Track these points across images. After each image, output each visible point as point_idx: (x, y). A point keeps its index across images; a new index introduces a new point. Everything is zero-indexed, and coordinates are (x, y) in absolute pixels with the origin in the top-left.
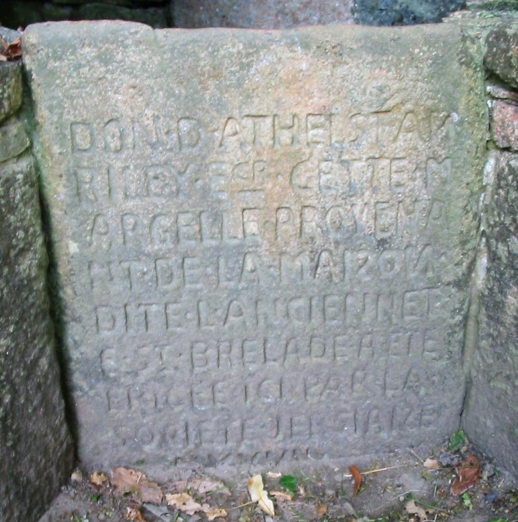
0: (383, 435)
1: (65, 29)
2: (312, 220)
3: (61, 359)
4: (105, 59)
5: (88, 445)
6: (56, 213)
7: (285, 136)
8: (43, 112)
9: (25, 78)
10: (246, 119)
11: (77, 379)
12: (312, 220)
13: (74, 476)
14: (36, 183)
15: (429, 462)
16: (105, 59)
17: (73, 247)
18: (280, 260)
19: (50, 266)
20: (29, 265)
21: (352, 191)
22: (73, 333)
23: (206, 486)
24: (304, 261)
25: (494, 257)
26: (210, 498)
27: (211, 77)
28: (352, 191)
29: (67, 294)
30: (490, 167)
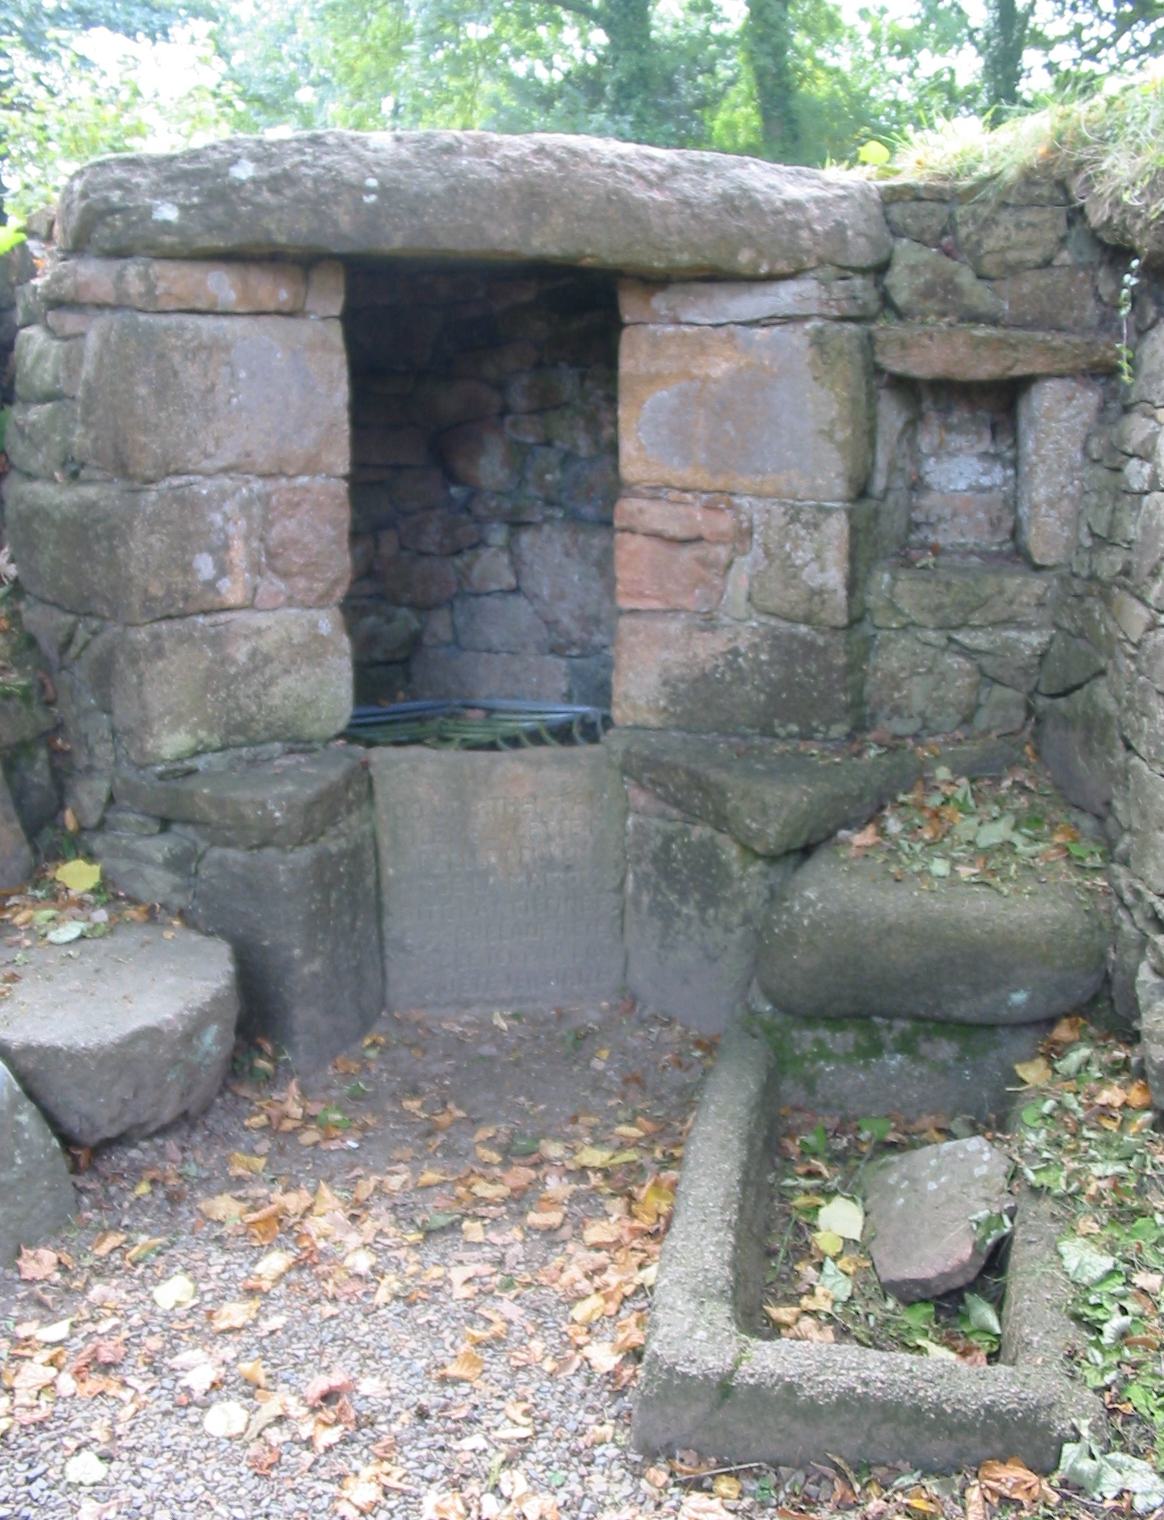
0: (576, 987)
1: (392, 753)
2: (527, 855)
3: (381, 938)
4: (414, 769)
5: (391, 994)
6: (383, 853)
7: (511, 809)
8: (379, 798)
9: (370, 780)
10: (1049, 562)
11: (389, 952)
12: (527, 855)
13: (384, 1013)
14: (374, 836)
15: (605, 1004)
16: (414, 769)
17: (391, 871)
18: (1101, 1281)
19: (378, 883)
20: (370, 881)
21: (549, 838)
22: (388, 921)
23: (466, 1018)
24: (522, 879)
25: (635, 874)
26: (467, 1024)
27: (938, 246)
28: (549, 838)
29: (386, 899)
30: (630, 822)
